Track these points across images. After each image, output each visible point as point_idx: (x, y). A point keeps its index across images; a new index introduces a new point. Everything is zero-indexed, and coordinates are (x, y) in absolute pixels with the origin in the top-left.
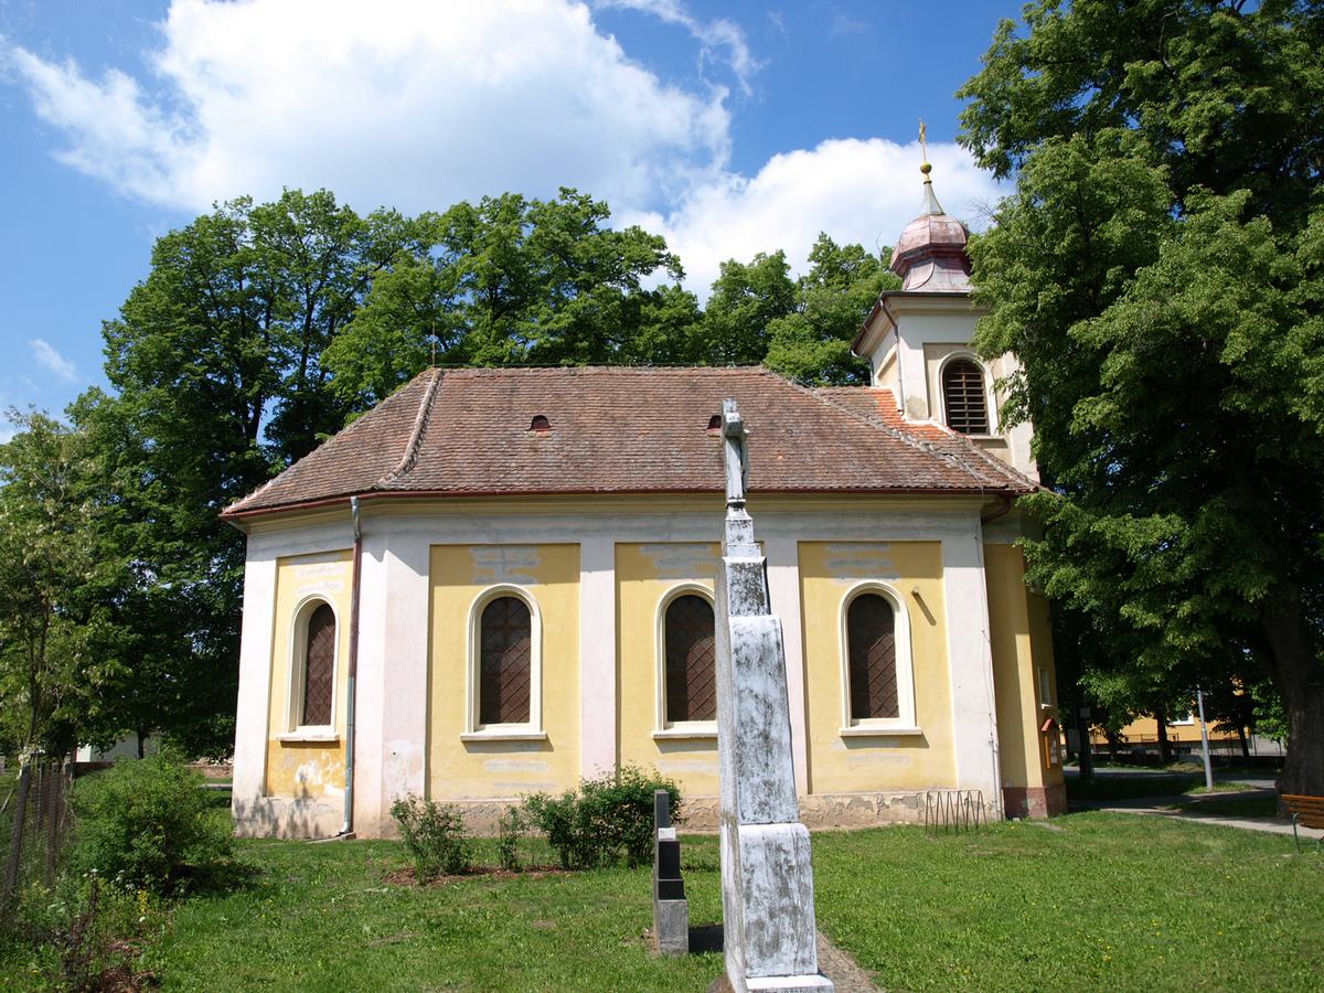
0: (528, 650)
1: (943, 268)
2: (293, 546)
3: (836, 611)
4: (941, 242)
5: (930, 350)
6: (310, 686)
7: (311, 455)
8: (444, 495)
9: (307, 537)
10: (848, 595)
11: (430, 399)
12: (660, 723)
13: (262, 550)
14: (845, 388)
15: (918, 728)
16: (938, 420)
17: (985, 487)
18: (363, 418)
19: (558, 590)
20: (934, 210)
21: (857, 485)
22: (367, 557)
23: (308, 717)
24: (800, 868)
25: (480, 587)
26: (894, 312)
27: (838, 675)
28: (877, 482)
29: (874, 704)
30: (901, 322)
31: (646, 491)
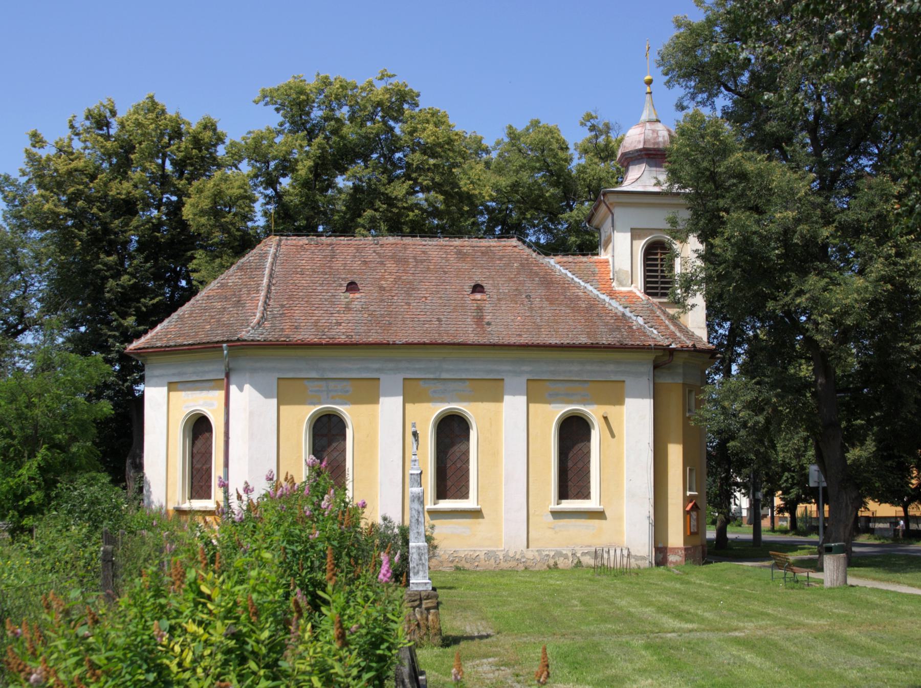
0: (344, 450)
1: (650, 166)
2: (180, 374)
3: (550, 429)
4: (652, 147)
5: (636, 234)
6: (195, 473)
7: (187, 305)
8: (287, 345)
9: (190, 369)
10: (559, 419)
11: (272, 264)
12: (431, 501)
13: (157, 376)
14: (575, 257)
15: (602, 507)
16: (638, 288)
17: (655, 345)
18: (222, 276)
19: (363, 409)
20: (651, 118)
21: (568, 342)
22: (233, 388)
23: (194, 494)
24: (425, 554)
25: (312, 407)
26: (611, 204)
27: (551, 471)
28: (583, 340)
29: (572, 490)
30: (617, 211)
31: (424, 344)
